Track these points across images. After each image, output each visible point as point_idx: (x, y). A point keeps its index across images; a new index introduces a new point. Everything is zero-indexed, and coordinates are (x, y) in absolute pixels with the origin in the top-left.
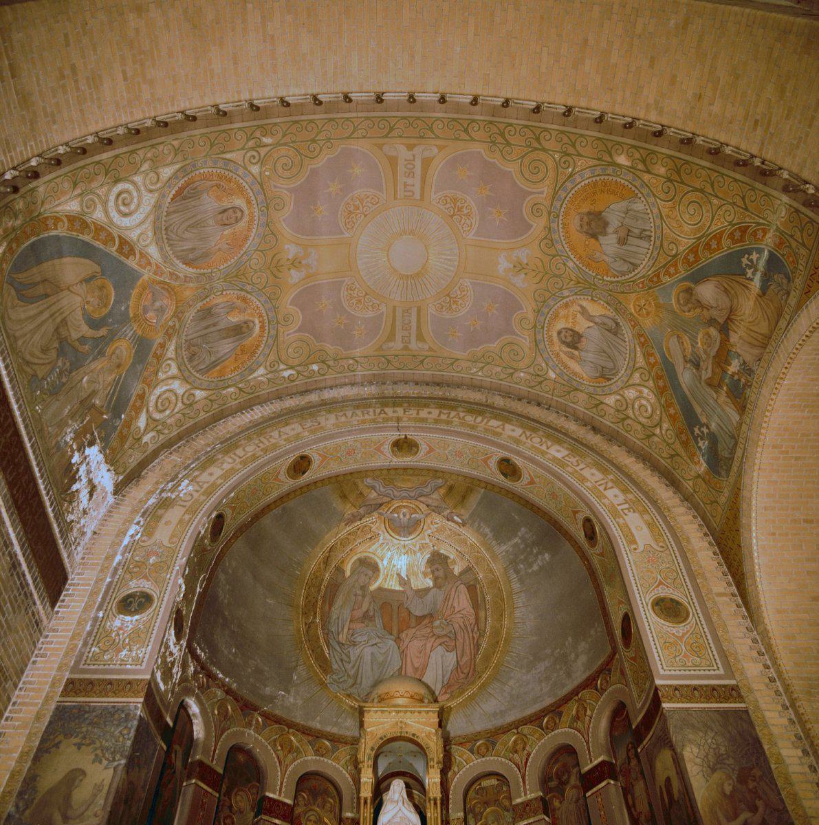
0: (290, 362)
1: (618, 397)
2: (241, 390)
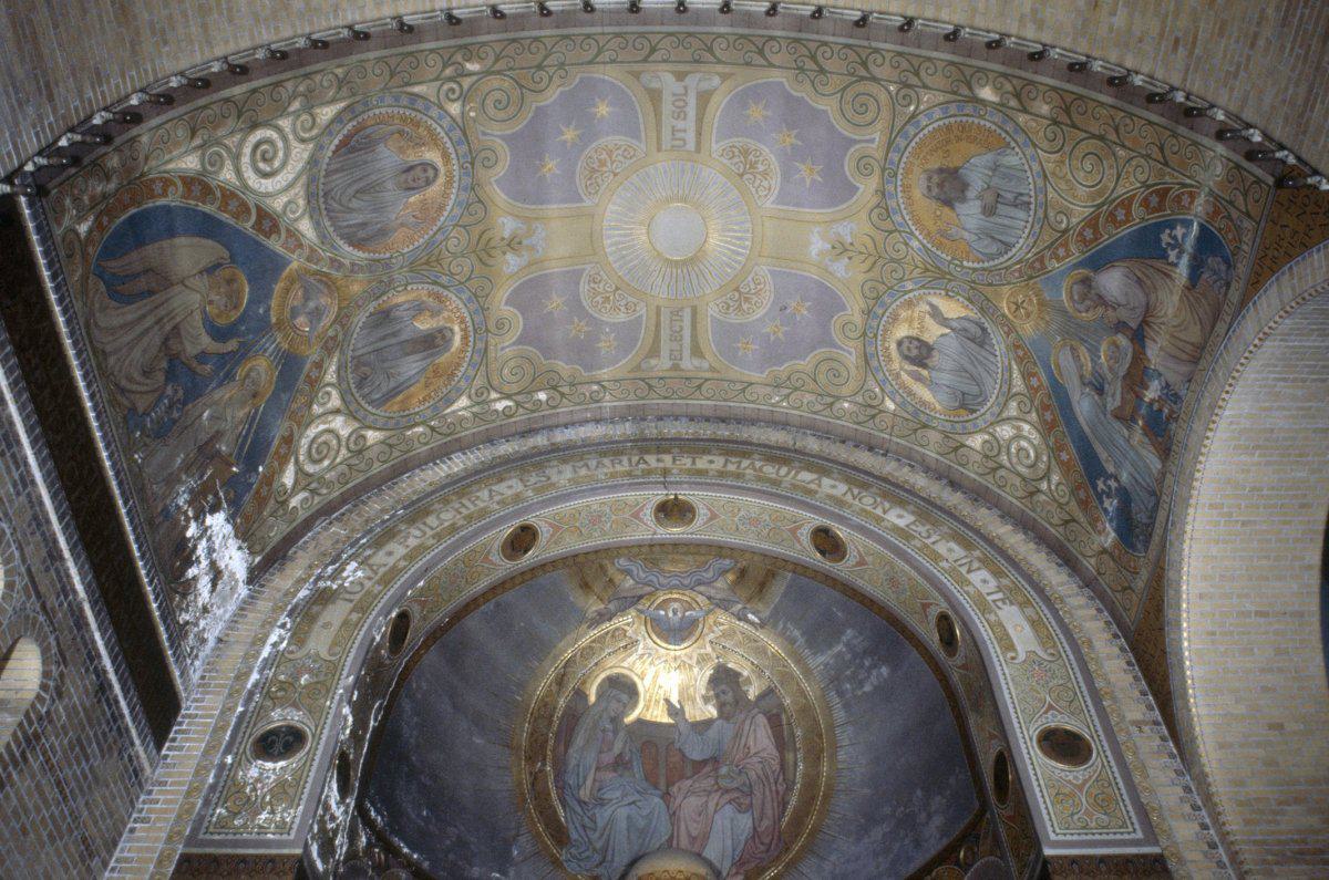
0: (506, 389)
1: (986, 437)
2: (433, 429)
